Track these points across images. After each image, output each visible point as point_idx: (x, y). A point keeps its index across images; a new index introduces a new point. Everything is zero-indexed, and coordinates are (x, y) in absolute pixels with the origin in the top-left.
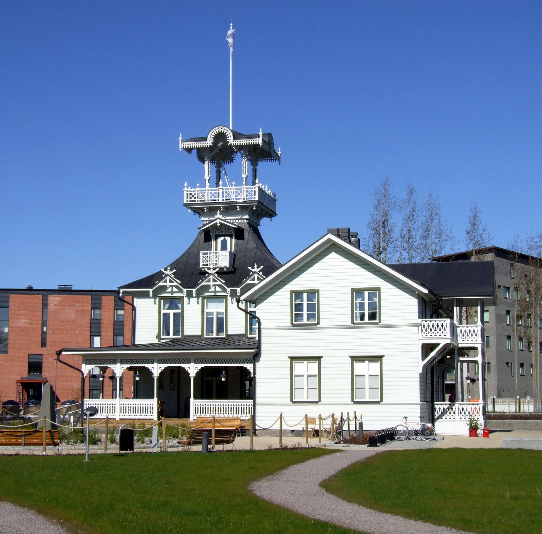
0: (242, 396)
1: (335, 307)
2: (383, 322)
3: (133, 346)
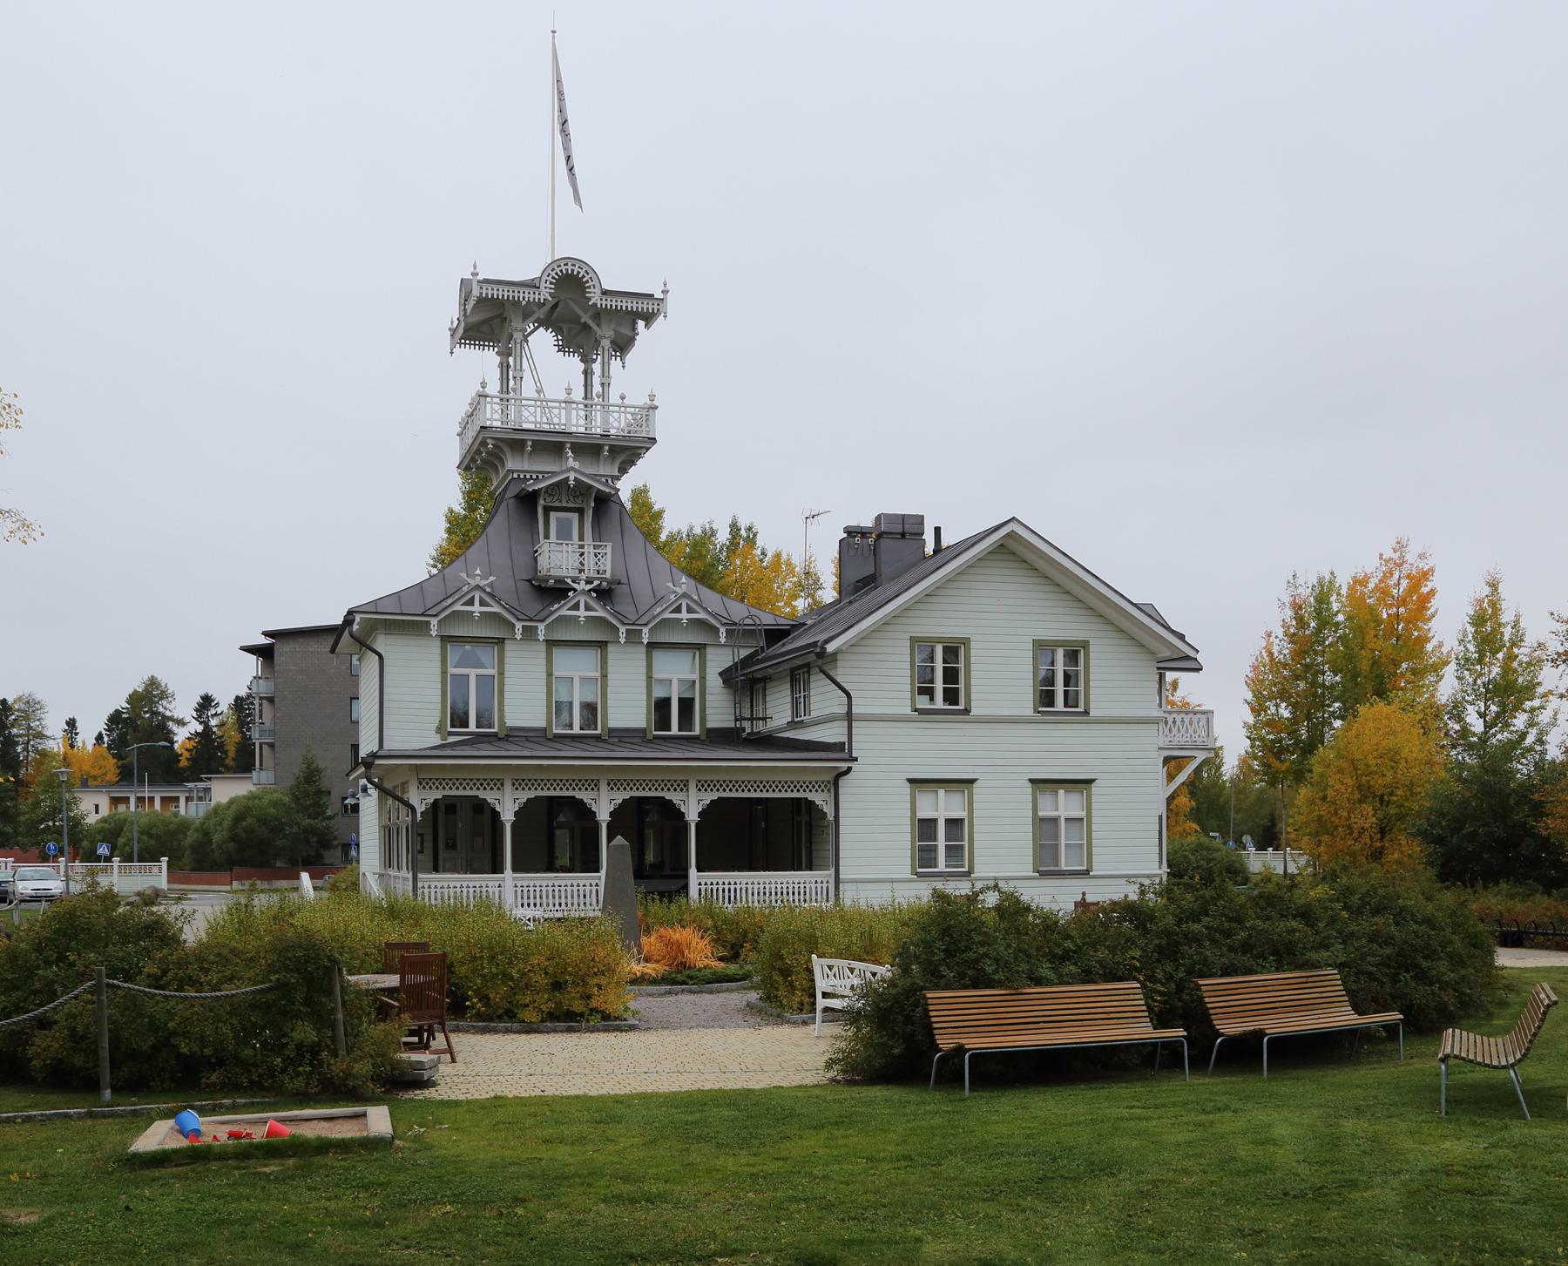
1: (1001, 678)
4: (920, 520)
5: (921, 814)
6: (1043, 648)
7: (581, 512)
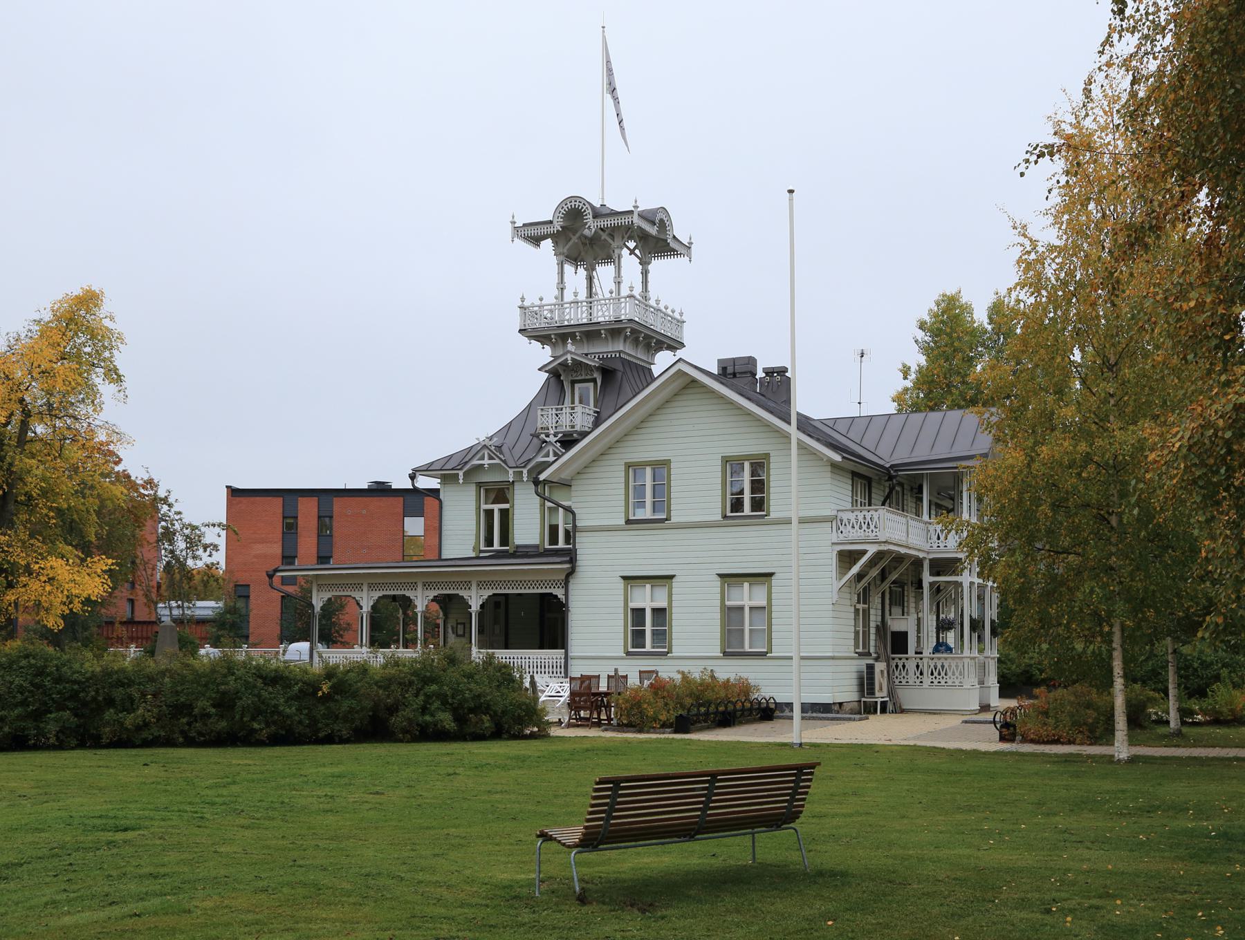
0: (553, 646)
1: (698, 492)
2: (773, 515)
3: (440, 559)
4: (751, 361)
5: (632, 605)
6: (731, 464)
7: (594, 381)
